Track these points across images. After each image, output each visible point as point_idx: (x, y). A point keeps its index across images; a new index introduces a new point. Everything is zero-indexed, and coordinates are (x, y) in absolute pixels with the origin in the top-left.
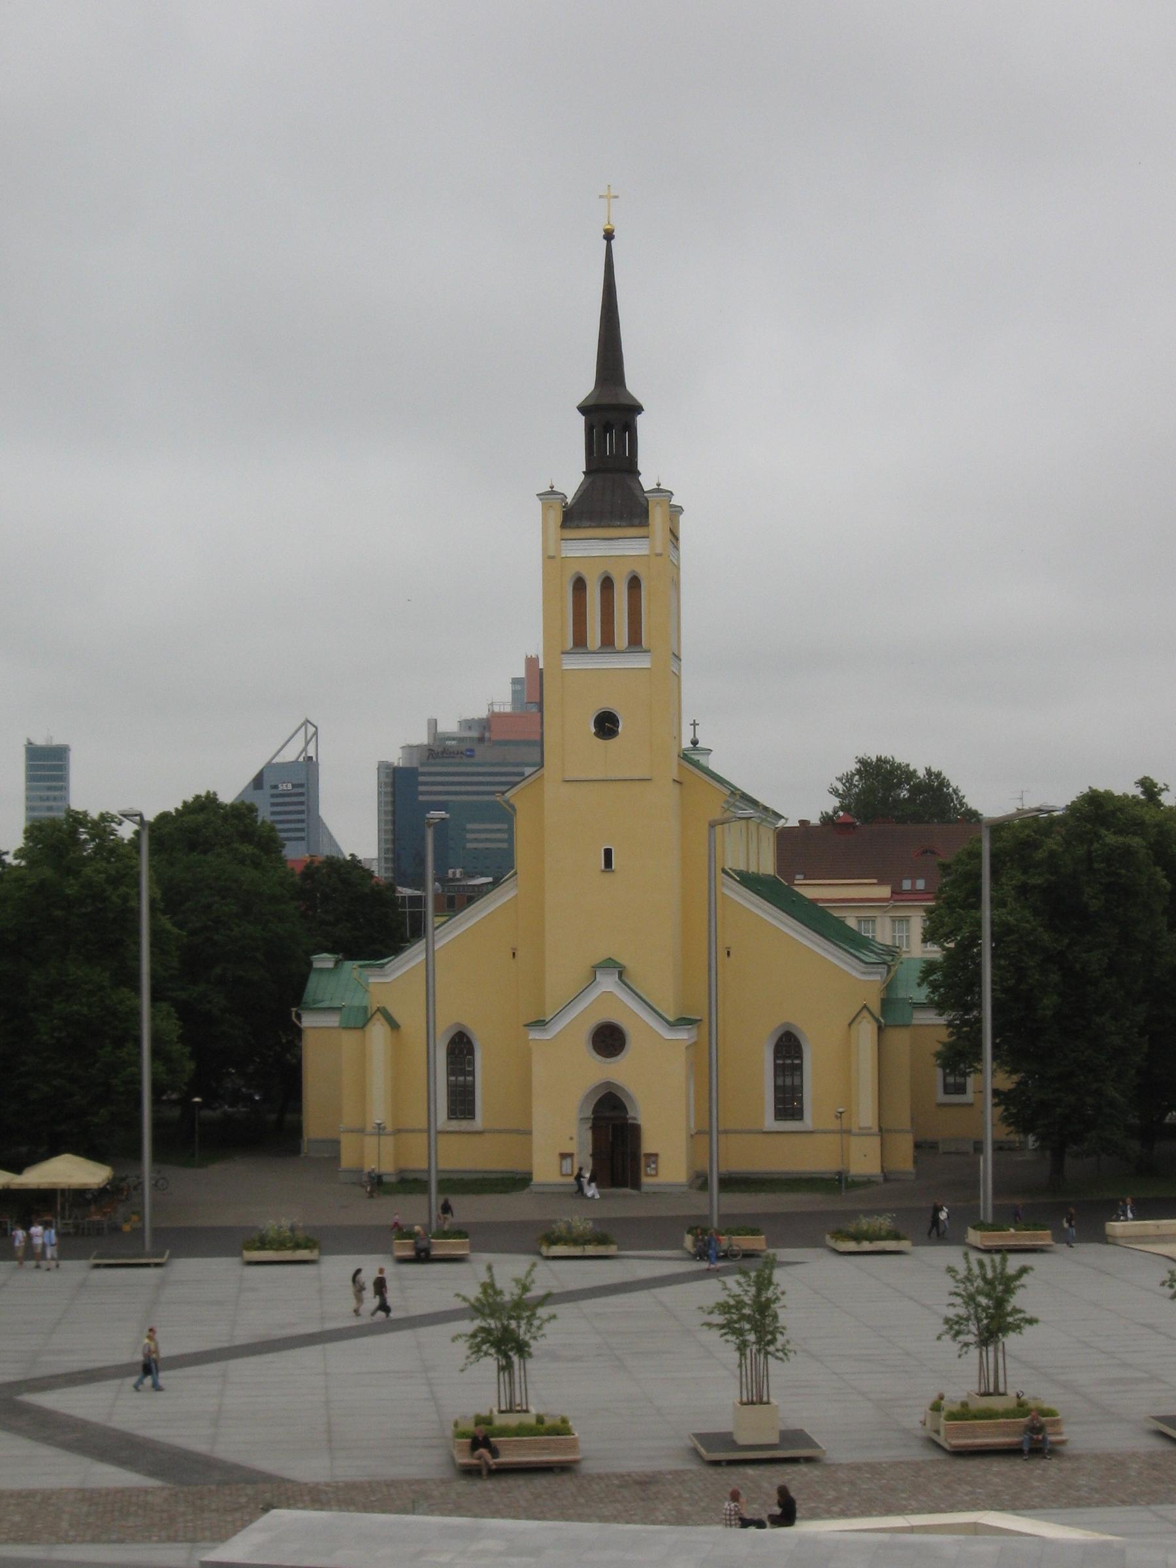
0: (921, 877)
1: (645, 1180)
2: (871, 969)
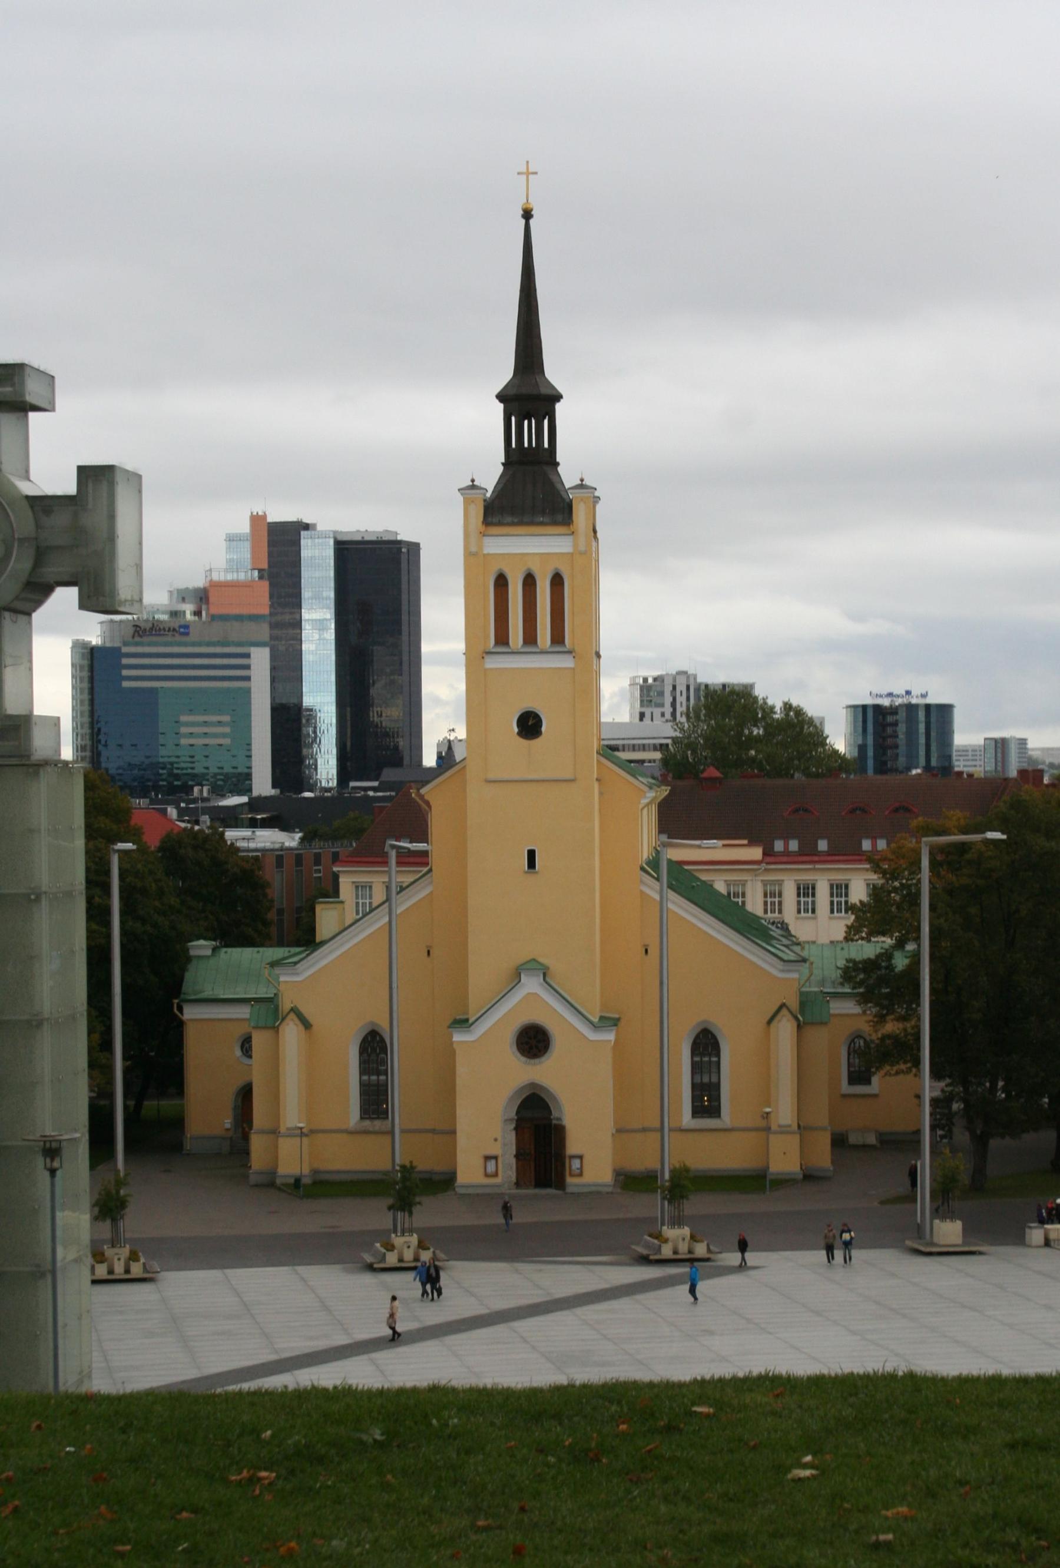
0: (793, 838)
1: (569, 1180)
2: (792, 967)
